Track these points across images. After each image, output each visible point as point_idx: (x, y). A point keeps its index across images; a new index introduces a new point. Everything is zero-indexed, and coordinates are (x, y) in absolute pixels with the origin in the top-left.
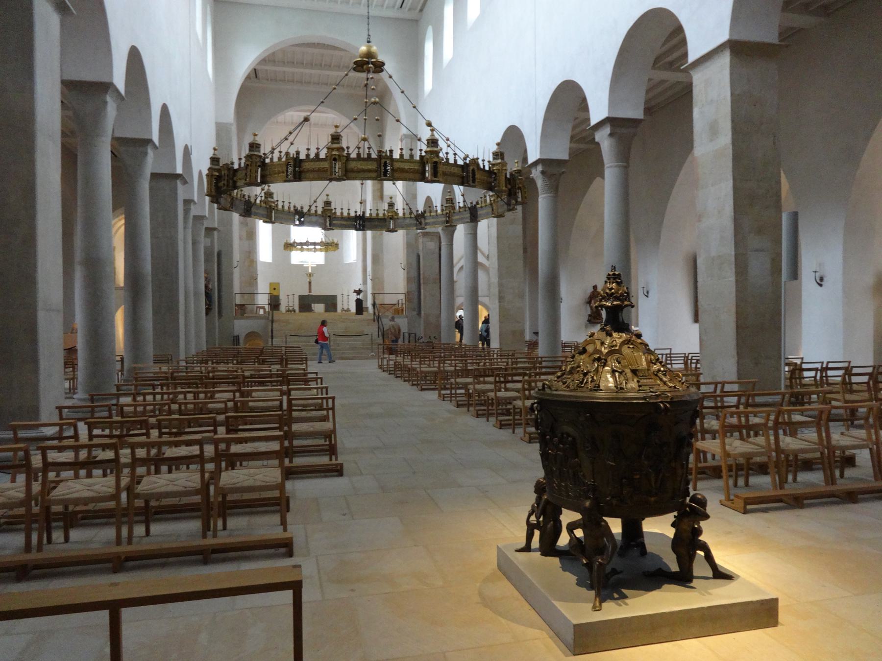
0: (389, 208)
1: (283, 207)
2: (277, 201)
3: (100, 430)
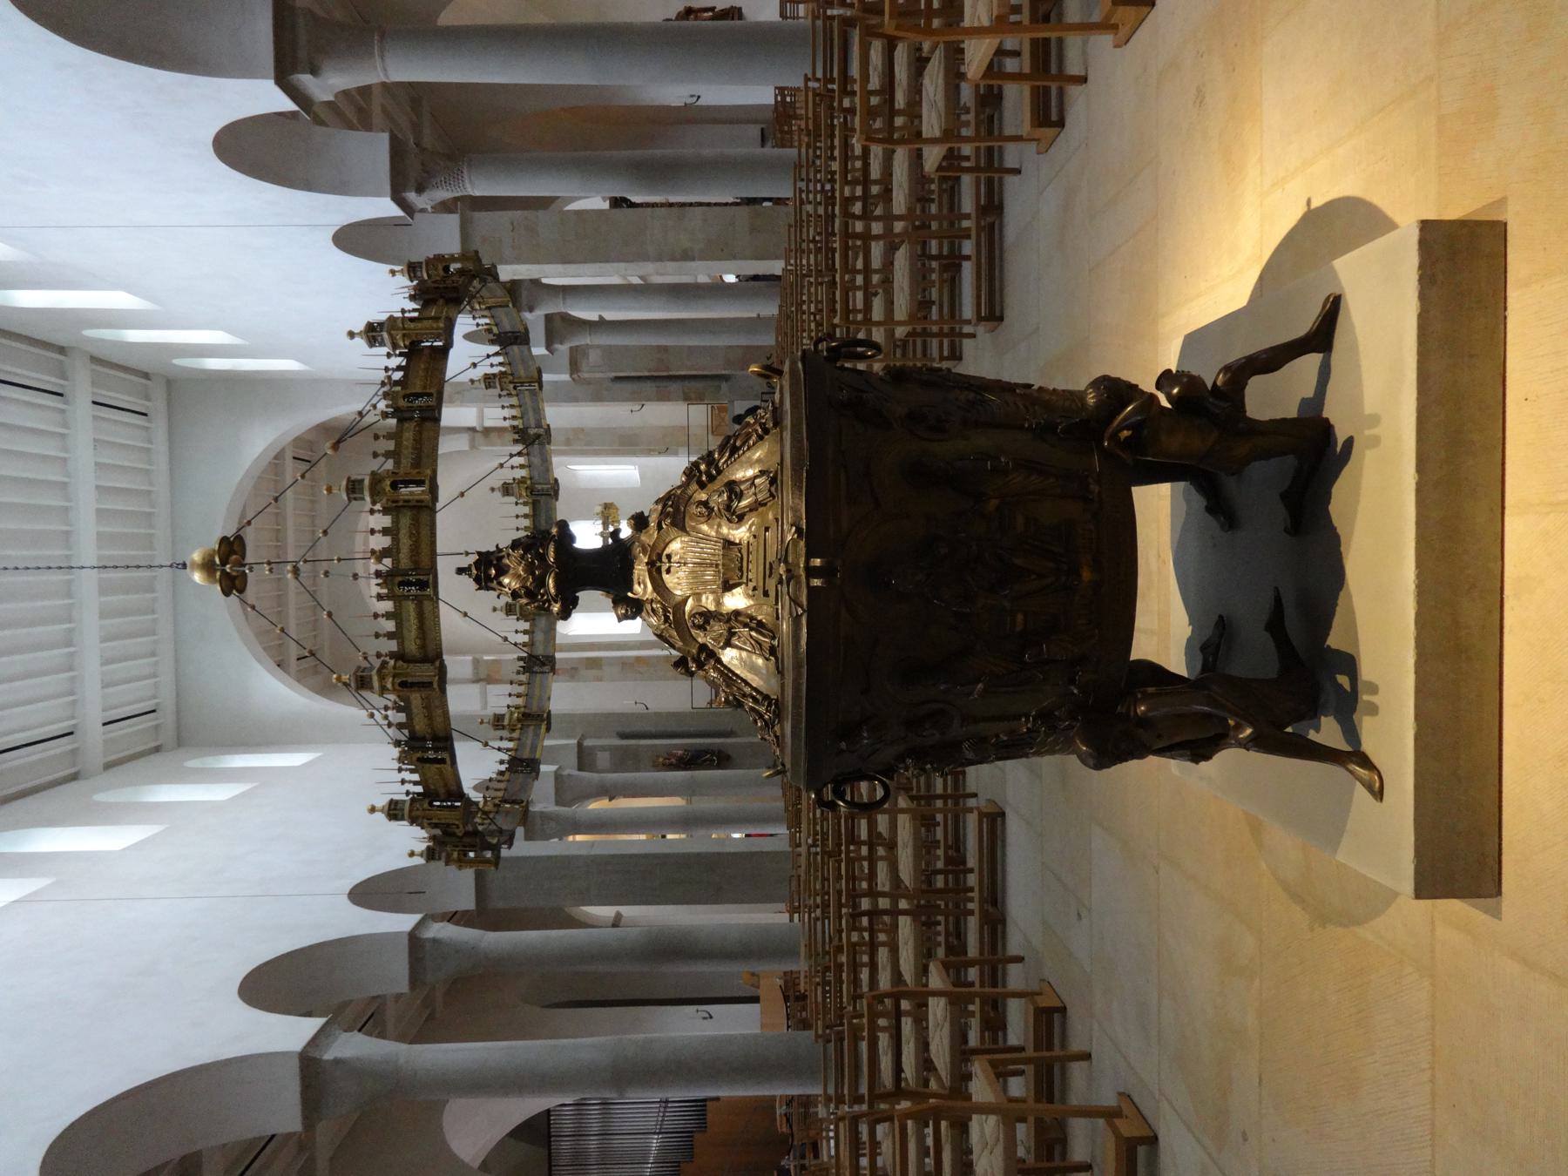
0: (513, 495)
1: (519, 696)
2: (508, 707)
3: (937, 828)
